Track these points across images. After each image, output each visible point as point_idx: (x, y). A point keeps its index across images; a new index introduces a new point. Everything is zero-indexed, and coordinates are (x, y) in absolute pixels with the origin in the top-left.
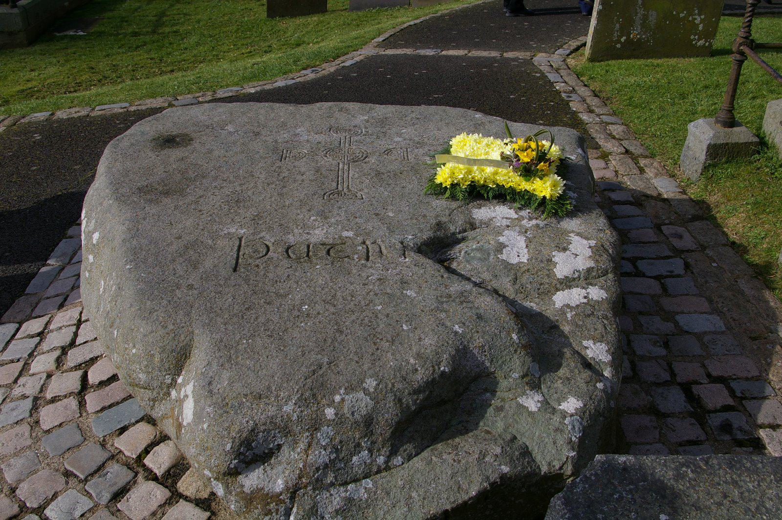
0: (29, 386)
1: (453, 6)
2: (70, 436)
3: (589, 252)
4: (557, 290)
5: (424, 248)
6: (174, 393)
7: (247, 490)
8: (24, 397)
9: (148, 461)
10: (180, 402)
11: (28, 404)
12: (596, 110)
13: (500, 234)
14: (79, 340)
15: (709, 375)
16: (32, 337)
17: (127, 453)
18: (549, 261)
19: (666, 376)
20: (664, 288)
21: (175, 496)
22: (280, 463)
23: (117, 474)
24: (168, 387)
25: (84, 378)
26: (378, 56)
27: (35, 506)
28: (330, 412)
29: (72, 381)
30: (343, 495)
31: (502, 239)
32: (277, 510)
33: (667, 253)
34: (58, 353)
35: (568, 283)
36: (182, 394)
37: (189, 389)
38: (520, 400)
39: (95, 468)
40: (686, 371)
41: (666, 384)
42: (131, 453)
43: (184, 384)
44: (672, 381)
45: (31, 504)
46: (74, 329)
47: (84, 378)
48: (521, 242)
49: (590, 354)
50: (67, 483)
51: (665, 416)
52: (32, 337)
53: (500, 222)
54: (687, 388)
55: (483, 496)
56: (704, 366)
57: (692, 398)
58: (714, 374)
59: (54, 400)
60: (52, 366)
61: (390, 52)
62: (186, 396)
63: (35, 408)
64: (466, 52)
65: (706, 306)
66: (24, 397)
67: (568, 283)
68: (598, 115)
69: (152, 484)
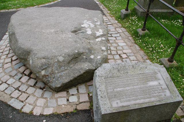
2: (10, 69)
29: (10, 60)
35: (98, 37)
53: (86, 27)
63: (3, 65)
67: (98, 37)
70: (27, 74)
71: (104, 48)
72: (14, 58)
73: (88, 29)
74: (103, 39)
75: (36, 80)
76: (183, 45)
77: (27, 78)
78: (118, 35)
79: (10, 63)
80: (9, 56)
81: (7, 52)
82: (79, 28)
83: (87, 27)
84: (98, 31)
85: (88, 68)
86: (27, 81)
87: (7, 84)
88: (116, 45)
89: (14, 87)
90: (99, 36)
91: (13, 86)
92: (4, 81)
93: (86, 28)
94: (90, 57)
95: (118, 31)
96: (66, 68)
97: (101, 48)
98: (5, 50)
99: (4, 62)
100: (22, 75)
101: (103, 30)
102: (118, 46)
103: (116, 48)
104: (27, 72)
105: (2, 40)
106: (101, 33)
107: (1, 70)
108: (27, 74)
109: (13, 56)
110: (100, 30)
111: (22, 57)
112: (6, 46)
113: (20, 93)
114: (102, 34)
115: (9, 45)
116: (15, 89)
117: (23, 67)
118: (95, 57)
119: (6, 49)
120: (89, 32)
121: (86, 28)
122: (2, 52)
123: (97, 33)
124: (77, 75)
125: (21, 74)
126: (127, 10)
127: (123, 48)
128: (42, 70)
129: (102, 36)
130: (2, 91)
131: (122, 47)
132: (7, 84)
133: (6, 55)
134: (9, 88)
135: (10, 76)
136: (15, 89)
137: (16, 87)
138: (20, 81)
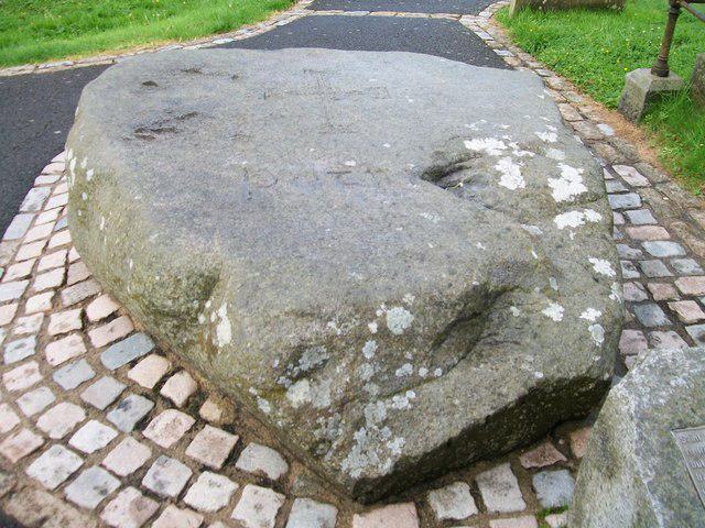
0: (29, 324)
1: (56, 64)
2: (84, 371)
3: (580, 179)
4: (557, 214)
5: (426, 176)
6: (202, 319)
7: (295, 406)
8: (26, 335)
9: (165, 391)
10: (212, 326)
11: (31, 342)
12: (531, 64)
13: (495, 163)
14: (70, 282)
15: (680, 293)
16: (21, 279)
17: (142, 384)
18: (546, 187)
19: (643, 296)
20: (627, 219)
21: (200, 423)
22: (325, 378)
23: (141, 406)
24: (197, 313)
25: (84, 315)
26: (308, 17)
27: (60, 437)
28: (373, 327)
29: (72, 319)
30: (388, 406)
31: (498, 168)
32: (327, 424)
33: (623, 189)
34: (52, 294)
35: (564, 207)
36: (213, 318)
37: (222, 311)
38: (543, 312)
39: (111, 400)
40: (660, 291)
41: (644, 302)
42: (148, 383)
43: (215, 308)
44: (651, 300)
45: (56, 435)
46: (63, 270)
47: (84, 315)
48: (516, 169)
49: (597, 269)
50: (87, 414)
51: (651, 329)
52: (21, 279)
53: (492, 152)
54: (663, 304)
55: (522, 401)
56: (674, 286)
57: (672, 315)
58: (685, 292)
59: (59, 336)
60: (48, 306)
61: (320, 13)
62: (219, 319)
63: (40, 347)
64: (394, 13)
65: (667, 235)
66: (26, 335)
67: (564, 207)
68: (533, 69)
69: (173, 413)
70: (179, 401)
71: (603, 267)
72: (98, 310)
73: (504, 165)
74: (593, 216)
75: (234, 433)
76: (283, 515)
77: (186, 421)
78: (634, 199)
79: (77, 338)
80: (67, 301)
81: (55, 278)
82: (454, 155)
83: (499, 153)
84: (558, 176)
85: (540, 375)
86: (182, 440)
87: (73, 449)
88: (634, 252)
89: (111, 472)
90: (570, 204)
91: (109, 466)
92: (56, 435)
93: (494, 160)
94: (543, 312)
95: (629, 180)
96: (423, 372)
97: (588, 267)
98: (40, 269)
99: (43, 329)
100: (150, 405)
101: (581, 171)
102: (647, 256)
103: (639, 269)
104: (178, 389)
105: (17, 213)
106: (579, 188)
107: (33, 371)
108: (179, 401)
109: (90, 299)
110: (569, 172)
111: (170, 303)
112: (43, 244)
113: (152, 505)
114: (584, 189)
115: (64, 238)
116: (118, 483)
117: (153, 358)
118: (571, 316)
119: (46, 262)
120: (512, 178)
121: (494, 160)
122: (28, 277)
123: (552, 183)
124: (483, 411)
125: (147, 397)
126: (662, 70)
127: (672, 269)
128: (295, 380)
129: (582, 201)
130: (49, 491)
131: (666, 261)
132: (73, 449)
133: (48, 290)
134: (85, 473)
135: (87, 407)
136: (118, 483)
137: (124, 472)
138: (143, 440)
